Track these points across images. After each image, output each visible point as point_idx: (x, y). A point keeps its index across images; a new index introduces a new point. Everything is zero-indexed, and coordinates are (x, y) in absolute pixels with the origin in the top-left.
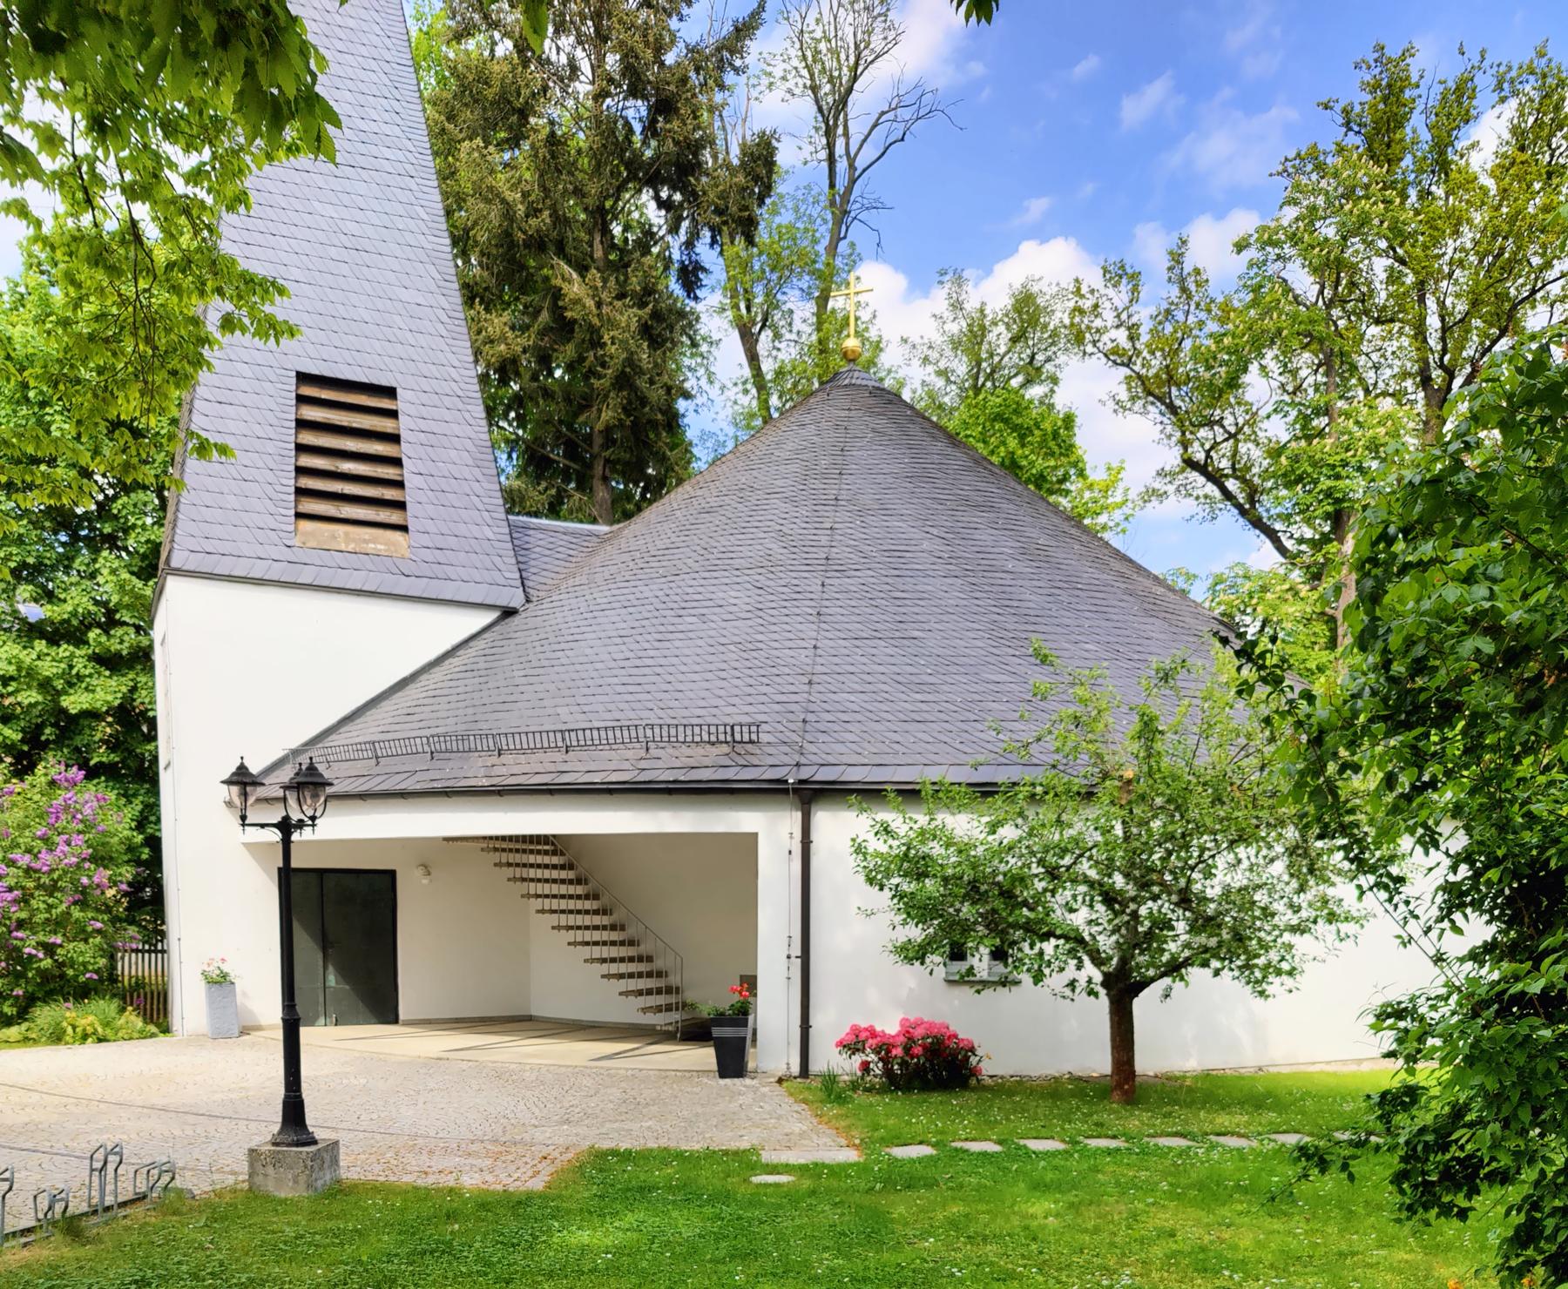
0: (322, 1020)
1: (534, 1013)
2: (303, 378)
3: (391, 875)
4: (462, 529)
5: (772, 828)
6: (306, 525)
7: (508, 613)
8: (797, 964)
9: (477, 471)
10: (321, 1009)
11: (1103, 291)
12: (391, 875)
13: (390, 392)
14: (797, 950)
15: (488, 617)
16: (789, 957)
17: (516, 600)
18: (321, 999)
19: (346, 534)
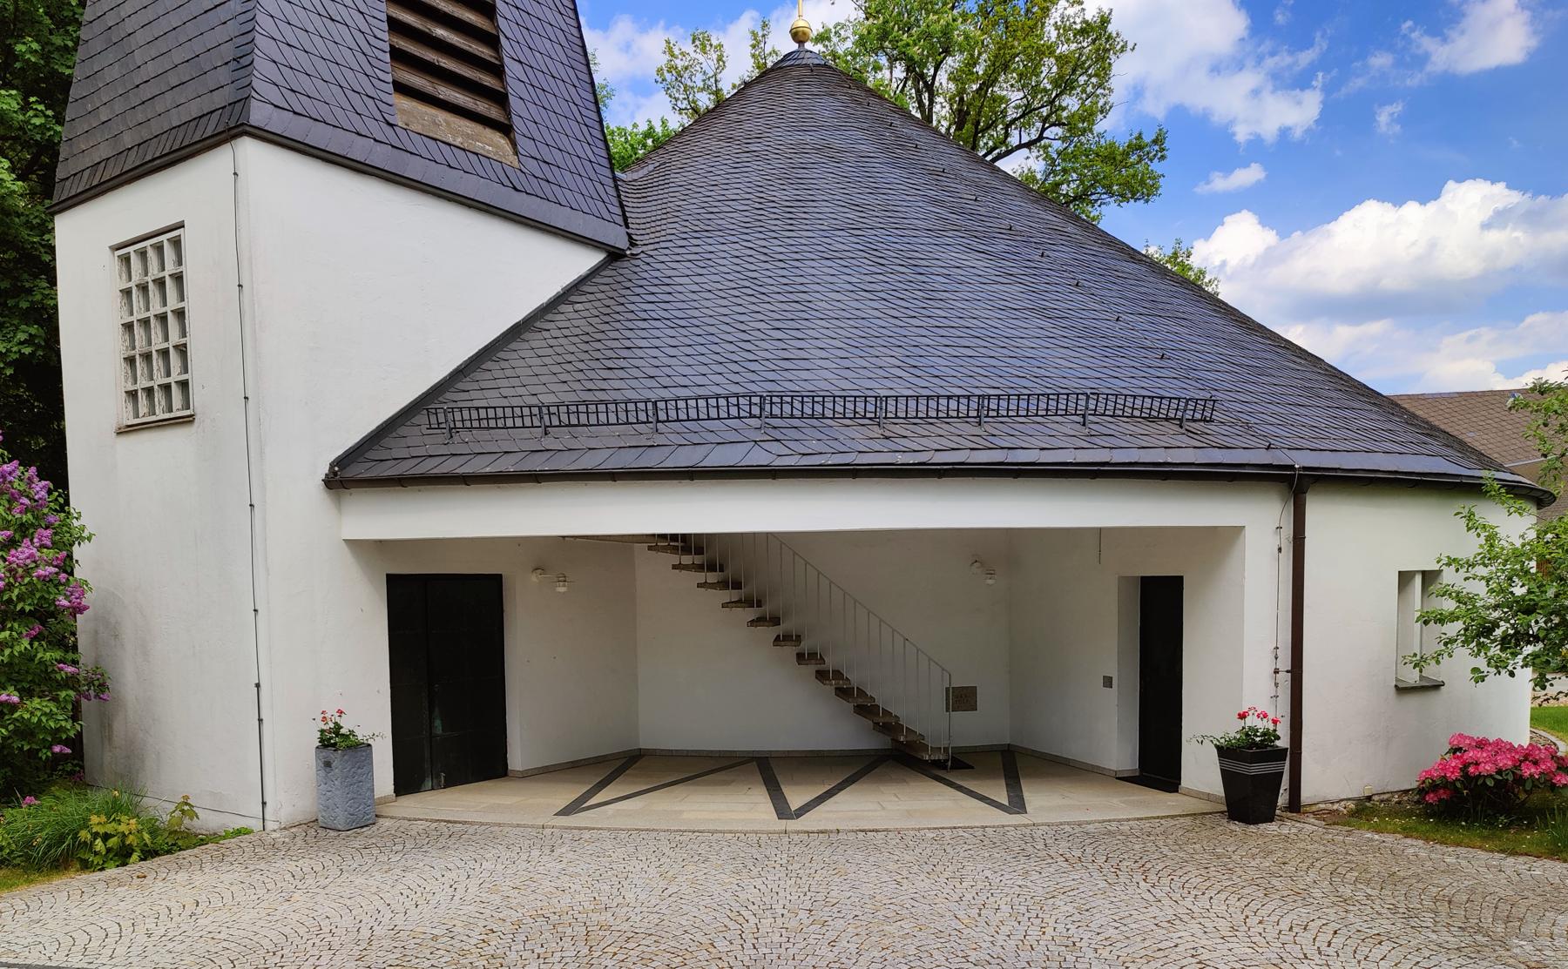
0: (429, 784)
1: (645, 743)
3: (497, 579)
4: (564, 142)
5: (1259, 521)
7: (615, 256)
8: (1285, 679)
9: (570, 71)
10: (427, 766)
11: (693, 55)
12: (1180, 579)
14: (1285, 663)
15: (585, 260)
16: (1276, 672)
17: (622, 243)
18: (427, 754)
19: (447, 123)
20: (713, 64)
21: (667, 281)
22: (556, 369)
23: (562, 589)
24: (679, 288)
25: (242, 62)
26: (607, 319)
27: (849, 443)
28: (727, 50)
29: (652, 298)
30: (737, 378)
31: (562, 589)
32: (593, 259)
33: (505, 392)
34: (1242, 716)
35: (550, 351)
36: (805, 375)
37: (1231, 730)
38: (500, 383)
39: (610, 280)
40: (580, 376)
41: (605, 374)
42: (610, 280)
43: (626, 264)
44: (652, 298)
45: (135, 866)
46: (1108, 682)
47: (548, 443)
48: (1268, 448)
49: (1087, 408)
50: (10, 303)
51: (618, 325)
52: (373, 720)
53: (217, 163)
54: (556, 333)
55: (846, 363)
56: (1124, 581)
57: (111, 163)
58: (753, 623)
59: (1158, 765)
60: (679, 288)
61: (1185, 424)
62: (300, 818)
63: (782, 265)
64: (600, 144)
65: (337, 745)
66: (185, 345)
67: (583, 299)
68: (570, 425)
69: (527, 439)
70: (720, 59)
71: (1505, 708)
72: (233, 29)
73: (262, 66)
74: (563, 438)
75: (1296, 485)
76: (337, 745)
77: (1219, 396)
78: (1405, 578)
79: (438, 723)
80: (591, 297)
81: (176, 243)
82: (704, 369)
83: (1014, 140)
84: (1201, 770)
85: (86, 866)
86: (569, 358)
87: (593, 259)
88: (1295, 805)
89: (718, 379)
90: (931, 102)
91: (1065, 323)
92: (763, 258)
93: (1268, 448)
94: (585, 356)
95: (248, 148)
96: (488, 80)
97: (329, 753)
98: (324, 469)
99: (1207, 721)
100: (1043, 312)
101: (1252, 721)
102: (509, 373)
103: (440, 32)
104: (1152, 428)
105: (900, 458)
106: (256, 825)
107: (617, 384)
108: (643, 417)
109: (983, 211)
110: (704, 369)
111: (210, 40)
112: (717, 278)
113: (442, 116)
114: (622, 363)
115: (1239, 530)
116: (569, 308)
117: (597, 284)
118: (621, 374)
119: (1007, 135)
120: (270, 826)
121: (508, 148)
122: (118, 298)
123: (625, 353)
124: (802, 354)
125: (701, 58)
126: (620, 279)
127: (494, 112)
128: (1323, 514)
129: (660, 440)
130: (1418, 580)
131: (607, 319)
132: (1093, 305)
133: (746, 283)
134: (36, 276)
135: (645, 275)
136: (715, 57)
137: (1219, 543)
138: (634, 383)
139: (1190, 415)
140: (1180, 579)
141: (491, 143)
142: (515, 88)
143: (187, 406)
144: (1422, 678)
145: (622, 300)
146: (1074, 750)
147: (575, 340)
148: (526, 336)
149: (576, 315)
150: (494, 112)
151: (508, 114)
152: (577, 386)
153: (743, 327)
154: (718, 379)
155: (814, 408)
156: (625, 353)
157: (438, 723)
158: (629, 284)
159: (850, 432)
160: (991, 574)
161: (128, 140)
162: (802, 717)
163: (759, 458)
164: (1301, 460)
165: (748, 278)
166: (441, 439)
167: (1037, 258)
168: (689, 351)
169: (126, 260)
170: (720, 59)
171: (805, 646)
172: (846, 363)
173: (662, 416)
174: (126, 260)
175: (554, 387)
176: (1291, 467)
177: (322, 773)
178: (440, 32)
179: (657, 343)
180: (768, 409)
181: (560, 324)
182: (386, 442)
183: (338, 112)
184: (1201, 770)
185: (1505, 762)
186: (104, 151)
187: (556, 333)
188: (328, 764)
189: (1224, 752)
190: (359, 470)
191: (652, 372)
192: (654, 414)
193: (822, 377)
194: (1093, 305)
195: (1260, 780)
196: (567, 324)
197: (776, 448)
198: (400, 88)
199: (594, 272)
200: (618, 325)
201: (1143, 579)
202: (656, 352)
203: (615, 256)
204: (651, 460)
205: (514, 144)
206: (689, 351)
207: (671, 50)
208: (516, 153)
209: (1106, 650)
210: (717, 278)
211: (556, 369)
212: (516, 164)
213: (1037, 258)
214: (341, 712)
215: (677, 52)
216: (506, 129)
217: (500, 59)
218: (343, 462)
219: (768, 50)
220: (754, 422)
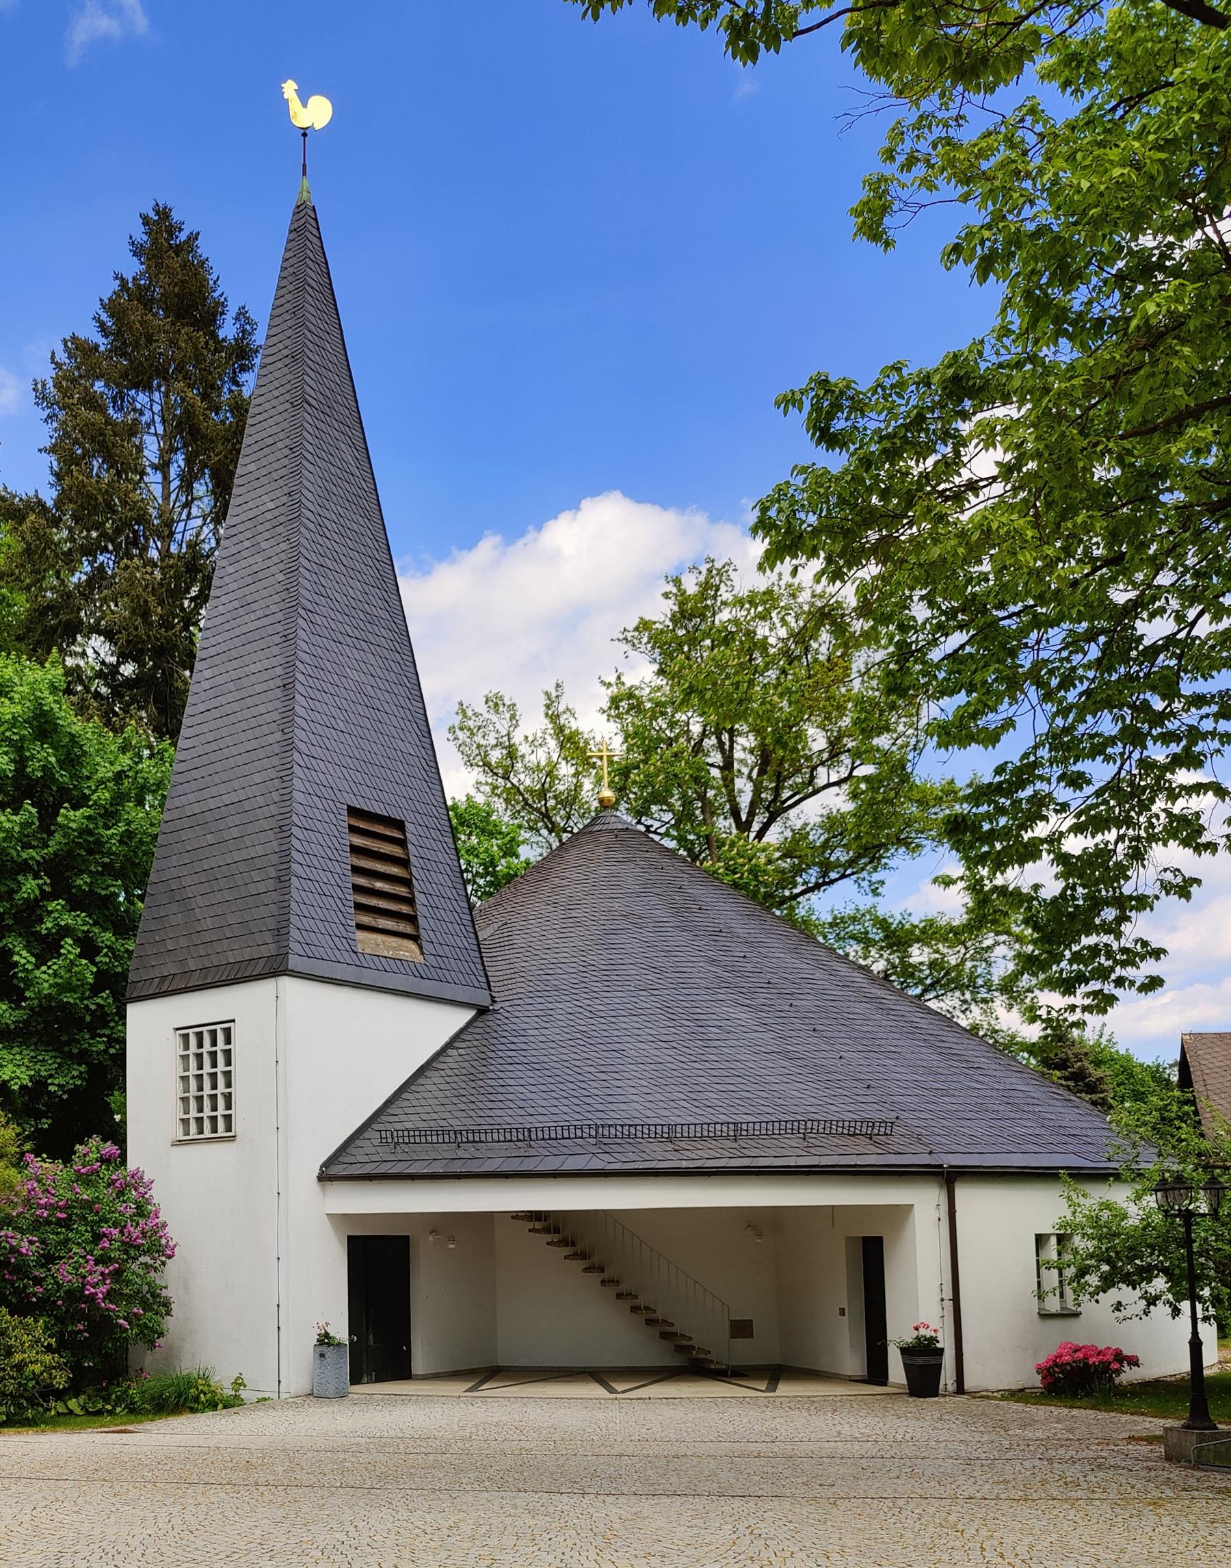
0: (365, 1379)
2: (353, 811)
3: (406, 1239)
5: (924, 1201)
6: (361, 935)
8: (949, 1305)
11: (486, 716)
12: (881, 1238)
13: (399, 825)
14: (948, 1294)
15: (466, 1016)
17: (486, 1002)
20: (506, 723)
21: (523, 1033)
22: (455, 1100)
23: (452, 1246)
24: (532, 1039)
25: (281, 932)
26: (484, 1062)
27: (652, 1154)
28: (520, 709)
29: (513, 1047)
30: (577, 1109)
31: (452, 1246)
32: (468, 1015)
33: (424, 1117)
34: (917, 1329)
35: (447, 1087)
36: (623, 1106)
37: (909, 1337)
38: (419, 1110)
39: (480, 1031)
40: (473, 1106)
41: (490, 1105)
42: (480, 1031)
43: (491, 1018)
44: (513, 1047)
45: (221, 1412)
46: (842, 1312)
47: (461, 1153)
48: (930, 1153)
49: (805, 1130)
50: (66, 1049)
51: (492, 1068)
52: (341, 1332)
53: (265, 989)
54: (450, 1072)
55: (650, 1098)
56: (850, 1240)
57: (178, 978)
58: (586, 1270)
59: (876, 1373)
60: (532, 1039)
61: (874, 1138)
62: (300, 1392)
63: (603, 1021)
64: (472, 936)
65: (325, 1340)
66: (230, 1094)
67: (463, 1045)
68: (474, 1142)
69: (447, 1151)
70: (513, 717)
71: (1160, 1337)
72: (274, 909)
73: (294, 933)
74: (468, 1151)
75: (949, 1178)
76: (325, 1340)
77: (903, 1115)
78: (1040, 1240)
79: (371, 1337)
80: (469, 1044)
81: (227, 1032)
82: (555, 1102)
83: (821, 780)
84: (897, 1371)
85: (193, 1411)
86: (463, 1092)
87: (468, 1015)
88: (960, 1389)
89: (565, 1109)
90: (732, 742)
91: (801, 1063)
92: (589, 1015)
93: (930, 1153)
94: (473, 1091)
95: (286, 983)
96: (405, 909)
97: (324, 1349)
98: (316, 1172)
99: (899, 1331)
100: (786, 1055)
101: (923, 1332)
102: (422, 1102)
103: (379, 885)
104: (850, 1141)
105: (684, 1164)
106: (275, 1396)
107: (499, 1112)
108: (521, 1137)
109: (749, 967)
110: (555, 1102)
111: (257, 914)
112: (557, 1031)
113: (380, 938)
114: (500, 1097)
115: (910, 1207)
116: (454, 1052)
117: (471, 1033)
118: (501, 1105)
119: (812, 778)
120: (283, 1396)
121: (417, 951)
122: (179, 1060)
123: (501, 1090)
124: (620, 1091)
125: (494, 718)
126: (488, 1030)
127: (409, 929)
128: (969, 1197)
129: (533, 1152)
130: (1053, 1240)
131: (484, 1062)
132: (827, 1047)
133: (579, 1036)
134: (81, 1030)
135: (506, 1027)
136: (508, 716)
137: (901, 1213)
138: (510, 1112)
139: (870, 1132)
140: (881, 1238)
141: (408, 950)
142: (422, 911)
143: (229, 1129)
144: (1062, 1308)
145: (493, 1048)
146: (824, 1365)
147: (464, 1078)
148: (427, 1073)
149: (460, 1059)
150: (409, 929)
151: (417, 928)
152: (472, 1113)
153: (579, 1070)
154: (565, 1109)
155: (631, 1133)
156: (501, 1090)
157: (371, 1337)
158: (495, 1035)
159: (654, 1147)
160: (760, 1235)
161: (192, 965)
162: (617, 1336)
163: (596, 1164)
164: (948, 1161)
165: (580, 1032)
166: (387, 1149)
167: (787, 1008)
168: (544, 1088)
169: (186, 1038)
170: (513, 717)
171: (624, 1288)
172: (650, 1098)
173: (533, 1137)
174: (186, 1038)
175: (458, 1114)
176: (941, 1166)
177: (318, 1362)
178: (379, 885)
179: (522, 1082)
180: (600, 1134)
181: (452, 1066)
182: (350, 1150)
183: (329, 951)
184: (897, 1371)
185: (1080, 1355)
186: (172, 969)
187: (450, 1072)
188: (322, 1355)
189: (905, 1351)
190: (335, 1170)
191: (521, 1104)
192: (528, 1137)
193: (634, 1105)
194: (827, 1047)
195: (926, 1370)
196: (455, 1065)
197: (606, 1157)
198: (360, 927)
199: (469, 1024)
200: (492, 1068)
201: (864, 1238)
202: (521, 1089)
203: (482, 1011)
204: (528, 1165)
205: (421, 948)
206: (544, 1088)
207: (464, 712)
208: (422, 953)
209: (838, 1290)
210: (557, 1031)
211: (455, 1100)
212: (423, 961)
213: (787, 1008)
214: (327, 1324)
215: (469, 713)
216: (415, 938)
217: (413, 894)
218: (327, 1164)
219: (562, 708)
220: (593, 1141)
